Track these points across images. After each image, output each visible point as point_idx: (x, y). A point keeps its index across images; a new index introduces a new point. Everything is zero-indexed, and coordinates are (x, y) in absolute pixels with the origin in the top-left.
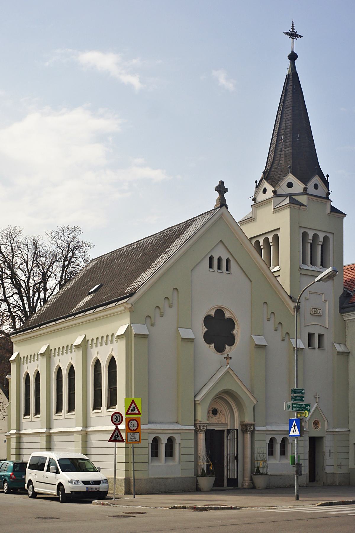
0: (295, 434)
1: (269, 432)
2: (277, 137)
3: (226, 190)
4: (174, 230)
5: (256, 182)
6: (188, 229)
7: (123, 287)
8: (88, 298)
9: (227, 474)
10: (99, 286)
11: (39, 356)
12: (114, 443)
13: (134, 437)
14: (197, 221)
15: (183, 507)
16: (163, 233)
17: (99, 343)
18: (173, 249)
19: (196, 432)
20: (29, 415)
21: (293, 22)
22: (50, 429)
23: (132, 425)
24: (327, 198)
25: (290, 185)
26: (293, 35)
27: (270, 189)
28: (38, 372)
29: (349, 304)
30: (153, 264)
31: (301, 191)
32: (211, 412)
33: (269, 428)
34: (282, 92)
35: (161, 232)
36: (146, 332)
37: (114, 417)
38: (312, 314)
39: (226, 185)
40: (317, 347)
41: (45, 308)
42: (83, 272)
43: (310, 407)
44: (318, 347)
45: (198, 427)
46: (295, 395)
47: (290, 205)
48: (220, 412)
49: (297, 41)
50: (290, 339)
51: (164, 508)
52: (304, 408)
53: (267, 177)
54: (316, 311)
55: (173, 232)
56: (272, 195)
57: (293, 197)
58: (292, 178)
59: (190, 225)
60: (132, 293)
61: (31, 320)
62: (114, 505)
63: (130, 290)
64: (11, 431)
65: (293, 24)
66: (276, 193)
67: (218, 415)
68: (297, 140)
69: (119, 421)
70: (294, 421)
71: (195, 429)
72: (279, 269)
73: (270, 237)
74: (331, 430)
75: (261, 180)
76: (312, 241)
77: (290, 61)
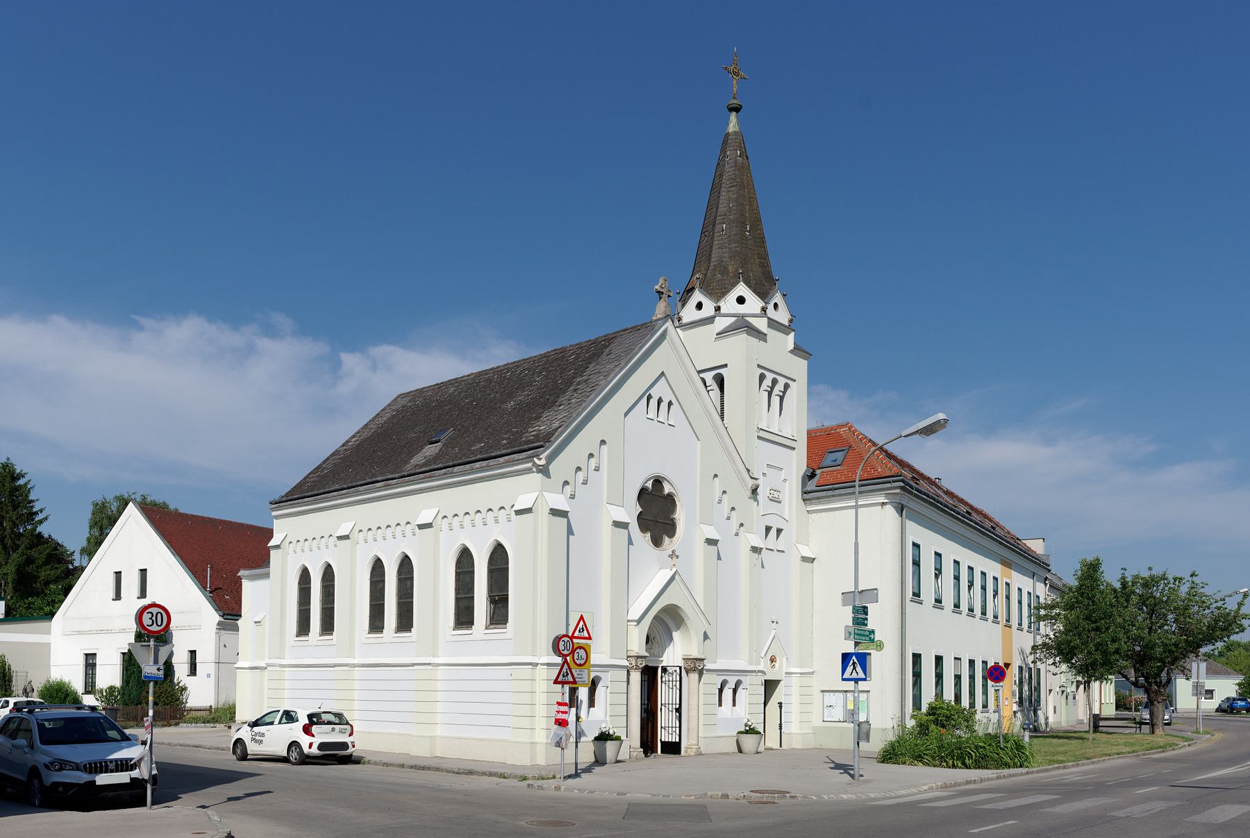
9: (664, 736)
12: (560, 686)
13: (580, 676)
16: (549, 356)
20: (307, 634)
25: (741, 300)
52: (867, 636)
57: (746, 318)
58: (744, 289)
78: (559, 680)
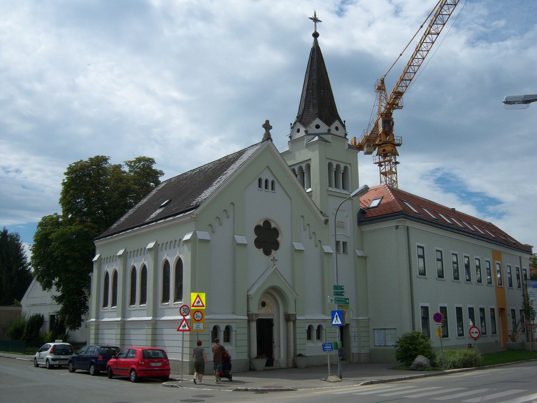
0: (337, 323)
1: (307, 321)
2: (307, 91)
3: (271, 128)
4: (229, 158)
5: (291, 124)
6: (241, 157)
7: (189, 201)
8: (159, 211)
10: (168, 201)
11: (117, 257)
13: (198, 326)
14: (248, 151)
15: (245, 389)
16: (221, 160)
17: (172, 246)
18: (230, 171)
19: (249, 321)
21: (315, 11)
22: (124, 318)
23: (197, 316)
24: (345, 138)
25: (318, 127)
26: (315, 20)
27: (302, 130)
28: (116, 270)
29: (365, 218)
30: (214, 183)
31: (326, 131)
32: (260, 304)
33: (308, 317)
34: (309, 59)
35: (219, 160)
36: (208, 238)
37: (182, 310)
38: (338, 226)
39: (271, 124)
40: (343, 252)
41: (124, 219)
42: (155, 191)
43: (348, 300)
44: (343, 252)
45: (251, 317)
46: (337, 291)
47: (318, 142)
48: (268, 304)
49: (318, 24)
50: (322, 246)
51: (228, 390)
52: (344, 301)
53: (300, 120)
54: (340, 224)
55: (228, 160)
56: (304, 134)
59: (243, 154)
60: (197, 205)
61: (112, 228)
62: (182, 387)
63: (195, 203)
64: (92, 319)
65: (315, 12)
66: (307, 133)
67: (266, 307)
68: (322, 94)
69: (186, 312)
70: (336, 312)
71: (248, 318)
72: (311, 190)
73: (304, 166)
74: (355, 318)
75: (295, 123)
76: (336, 169)
77: (313, 38)
78: (180, 329)
